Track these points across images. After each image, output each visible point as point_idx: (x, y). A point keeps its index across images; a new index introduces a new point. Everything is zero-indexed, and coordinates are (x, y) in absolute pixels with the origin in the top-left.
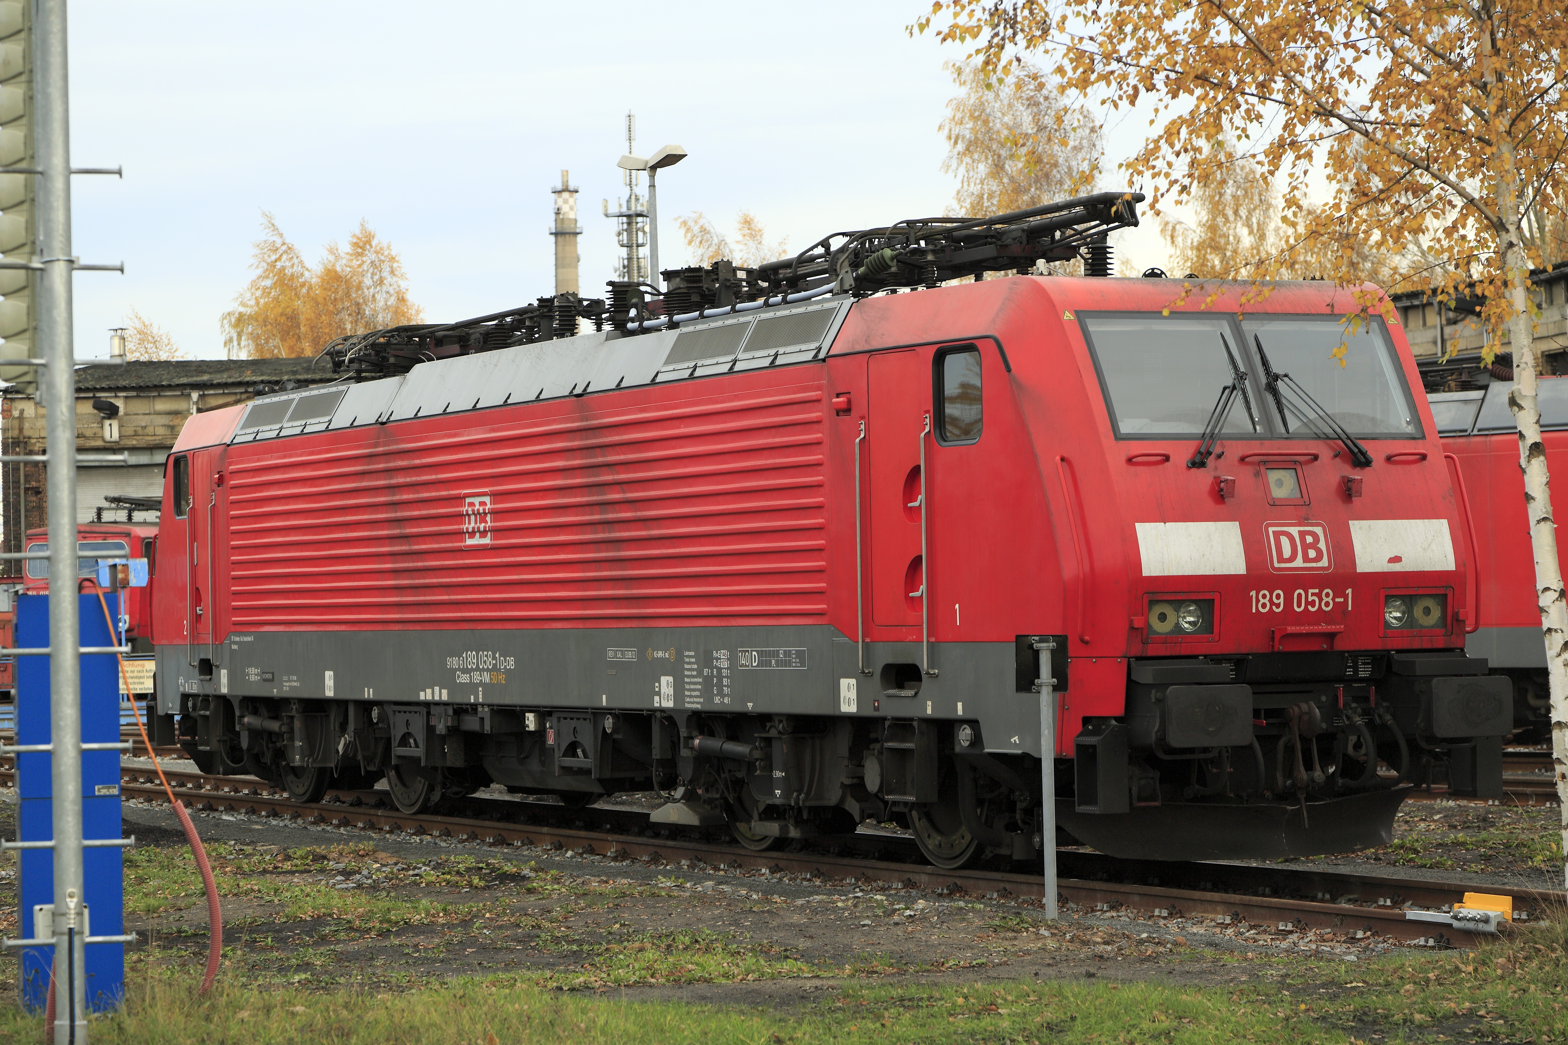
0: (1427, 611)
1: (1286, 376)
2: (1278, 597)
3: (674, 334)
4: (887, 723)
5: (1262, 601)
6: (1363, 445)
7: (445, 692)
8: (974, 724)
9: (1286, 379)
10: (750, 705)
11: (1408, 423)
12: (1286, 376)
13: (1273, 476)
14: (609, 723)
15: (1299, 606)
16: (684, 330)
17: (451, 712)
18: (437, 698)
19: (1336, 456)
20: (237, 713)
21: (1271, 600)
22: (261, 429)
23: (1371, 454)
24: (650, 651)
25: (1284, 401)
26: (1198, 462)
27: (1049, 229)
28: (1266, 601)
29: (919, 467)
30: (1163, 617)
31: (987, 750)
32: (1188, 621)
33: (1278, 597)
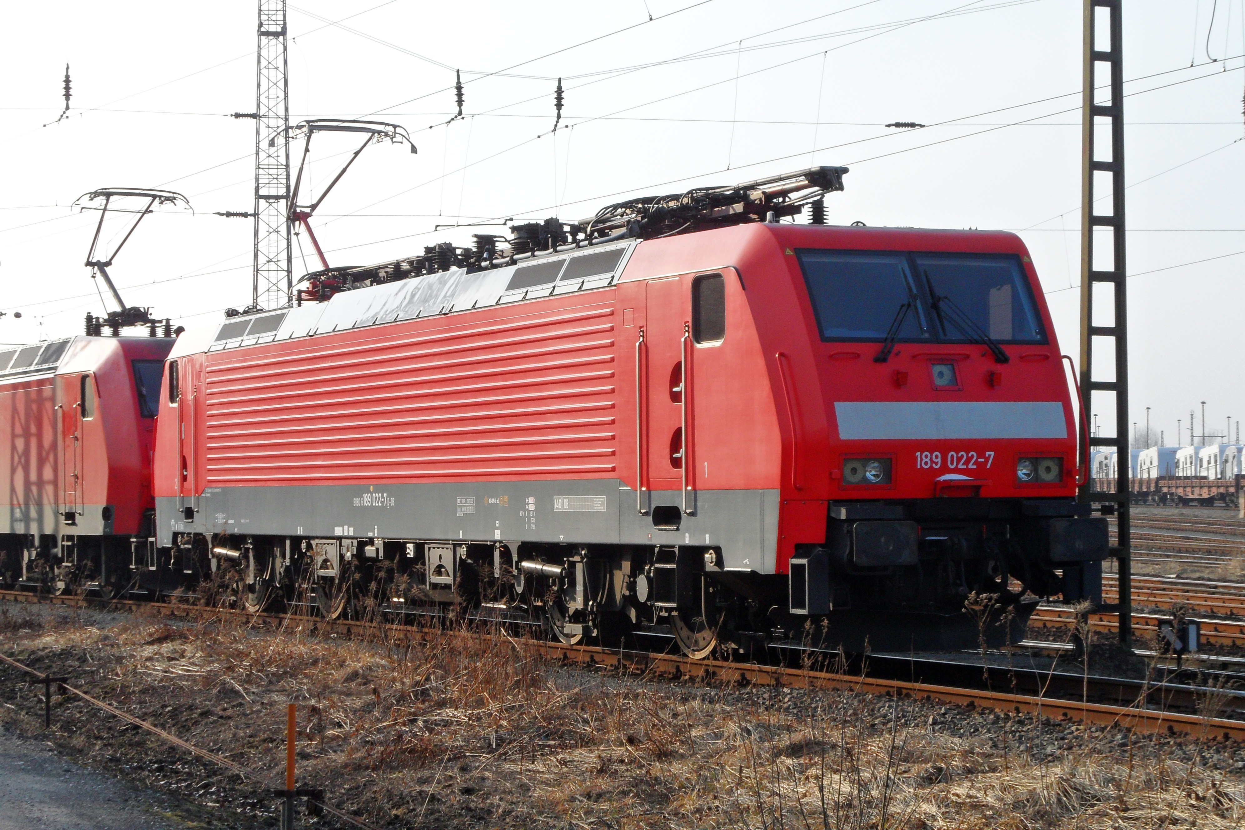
0: (1048, 469)
1: (946, 298)
2: (937, 457)
3: (513, 269)
4: (657, 550)
5: (925, 460)
6: (1003, 347)
7: (351, 529)
8: (718, 550)
9: (947, 301)
10: (562, 537)
11: (1037, 333)
12: (946, 298)
13: (937, 369)
14: (463, 551)
15: (952, 463)
16: (521, 265)
17: (355, 544)
18: (346, 534)
19: (983, 356)
20: (210, 546)
21: (931, 460)
22: (228, 341)
23: (1007, 353)
24: (486, 498)
25: (942, 314)
26: (881, 359)
27: (784, 193)
28: (928, 460)
29: (680, 363)
30: (854, 471)
31: (726, 569)
32: (872, 474)
33: (937, 457)
